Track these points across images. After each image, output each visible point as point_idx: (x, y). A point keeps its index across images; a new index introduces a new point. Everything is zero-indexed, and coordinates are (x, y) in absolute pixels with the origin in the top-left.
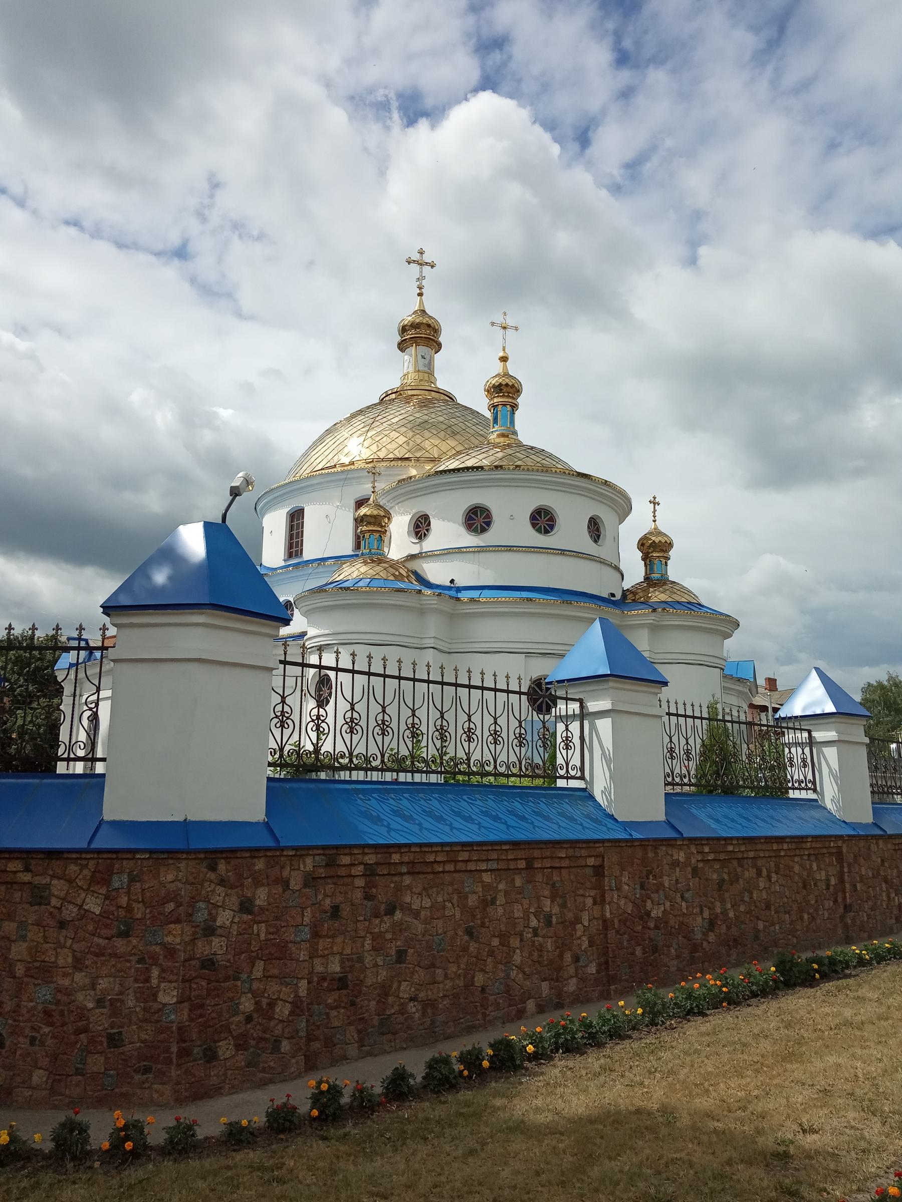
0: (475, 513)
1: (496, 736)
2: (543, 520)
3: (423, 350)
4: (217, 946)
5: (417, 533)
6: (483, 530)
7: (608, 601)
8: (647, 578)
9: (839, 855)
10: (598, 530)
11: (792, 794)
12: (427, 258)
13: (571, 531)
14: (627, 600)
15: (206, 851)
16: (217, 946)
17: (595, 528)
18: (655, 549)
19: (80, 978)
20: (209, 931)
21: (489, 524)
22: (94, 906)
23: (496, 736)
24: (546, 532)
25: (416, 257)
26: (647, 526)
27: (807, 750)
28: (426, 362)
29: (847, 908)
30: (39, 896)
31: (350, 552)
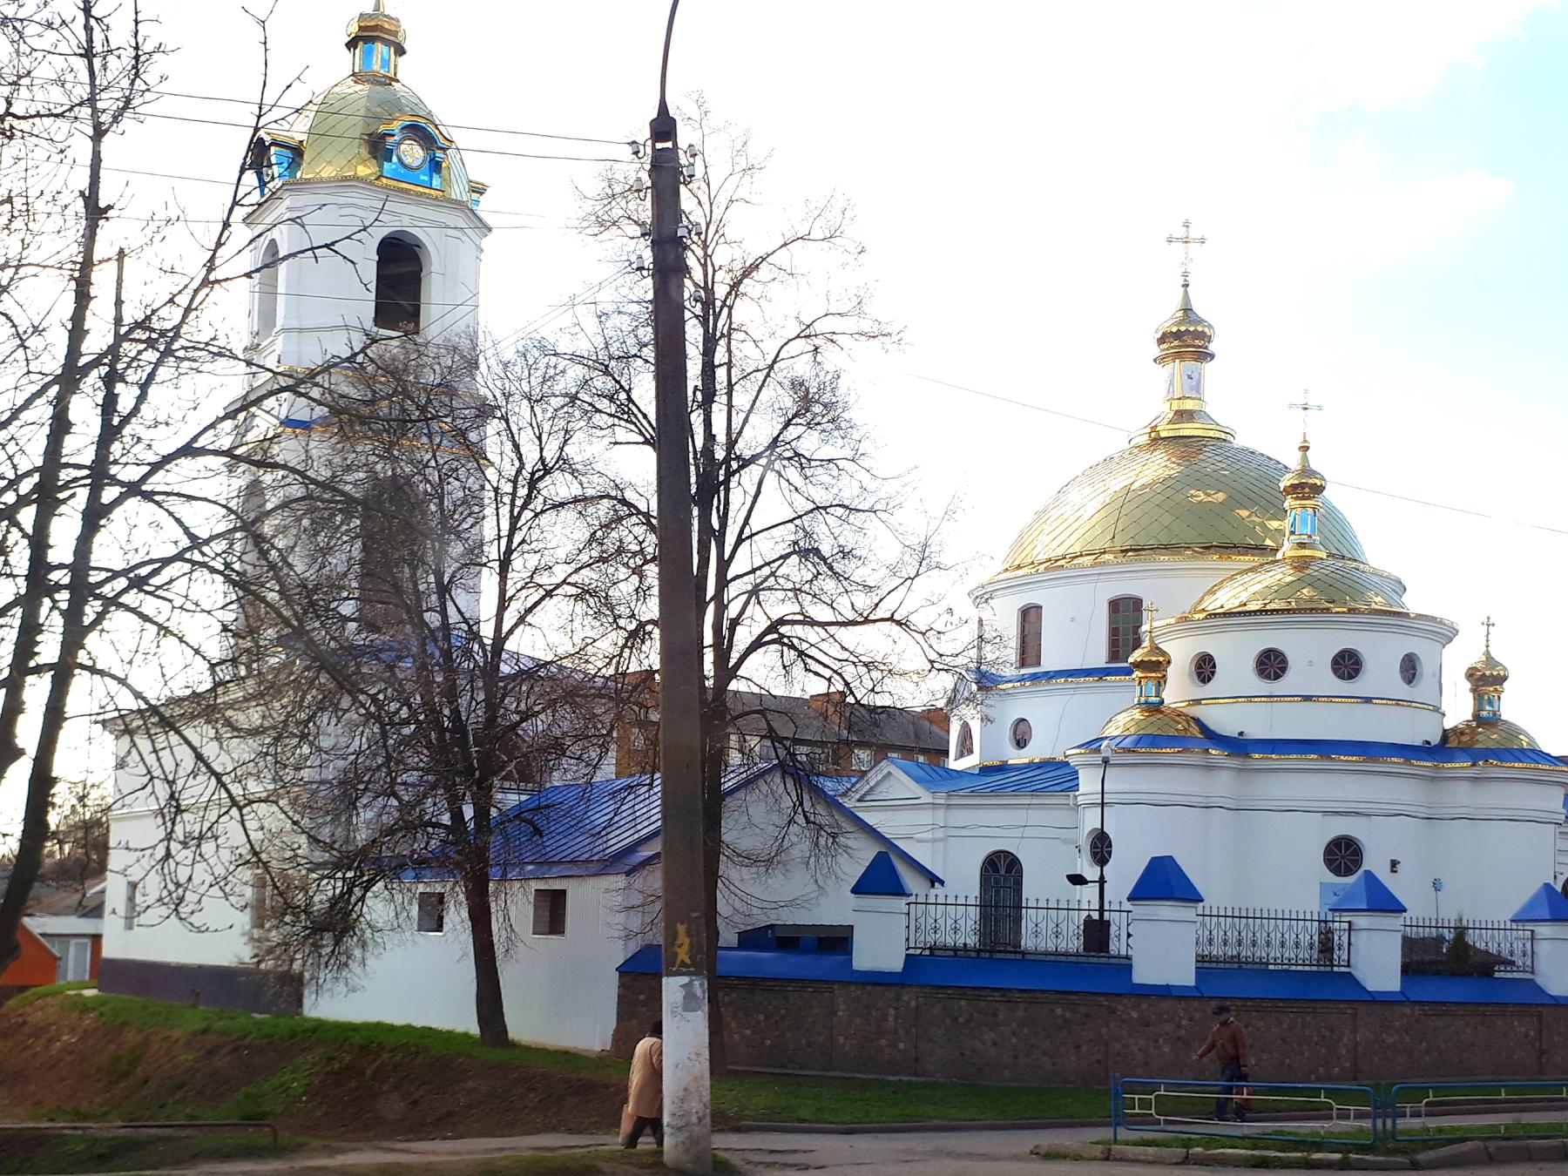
0: (1268, 657)
1: (1297, 945)
2: (1347, 664)
3: (1191, 365)
4: (1183, 1032)
5: (1199, 674)
6: (1277, 677)
7: (1425, 751)
8: (1476, 716)
9: (1540, 1015)
10: (1414, 668)
11: (1497, 975)
12: (1194, 233)
13: (1380, 674)
14: (1447, 747)
15: (1465, 974)
16: (1183, 1032)
17: (1410, 668)
18: (1486, 680)
19: (1132, 1041)
20: (1180, 1026)
21: (1284, 670)
22: (1135, 1015)
23: (1297, 945)
24: (1351, 677)
25: (1180, 232)
26: (1474, 657)
27: (1529, 944)
28: (1194, 383)
29: (1542, 1052)
30: (1113, 1011)
31: (1099, 658)
